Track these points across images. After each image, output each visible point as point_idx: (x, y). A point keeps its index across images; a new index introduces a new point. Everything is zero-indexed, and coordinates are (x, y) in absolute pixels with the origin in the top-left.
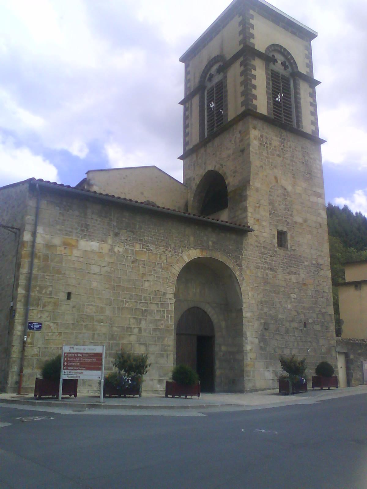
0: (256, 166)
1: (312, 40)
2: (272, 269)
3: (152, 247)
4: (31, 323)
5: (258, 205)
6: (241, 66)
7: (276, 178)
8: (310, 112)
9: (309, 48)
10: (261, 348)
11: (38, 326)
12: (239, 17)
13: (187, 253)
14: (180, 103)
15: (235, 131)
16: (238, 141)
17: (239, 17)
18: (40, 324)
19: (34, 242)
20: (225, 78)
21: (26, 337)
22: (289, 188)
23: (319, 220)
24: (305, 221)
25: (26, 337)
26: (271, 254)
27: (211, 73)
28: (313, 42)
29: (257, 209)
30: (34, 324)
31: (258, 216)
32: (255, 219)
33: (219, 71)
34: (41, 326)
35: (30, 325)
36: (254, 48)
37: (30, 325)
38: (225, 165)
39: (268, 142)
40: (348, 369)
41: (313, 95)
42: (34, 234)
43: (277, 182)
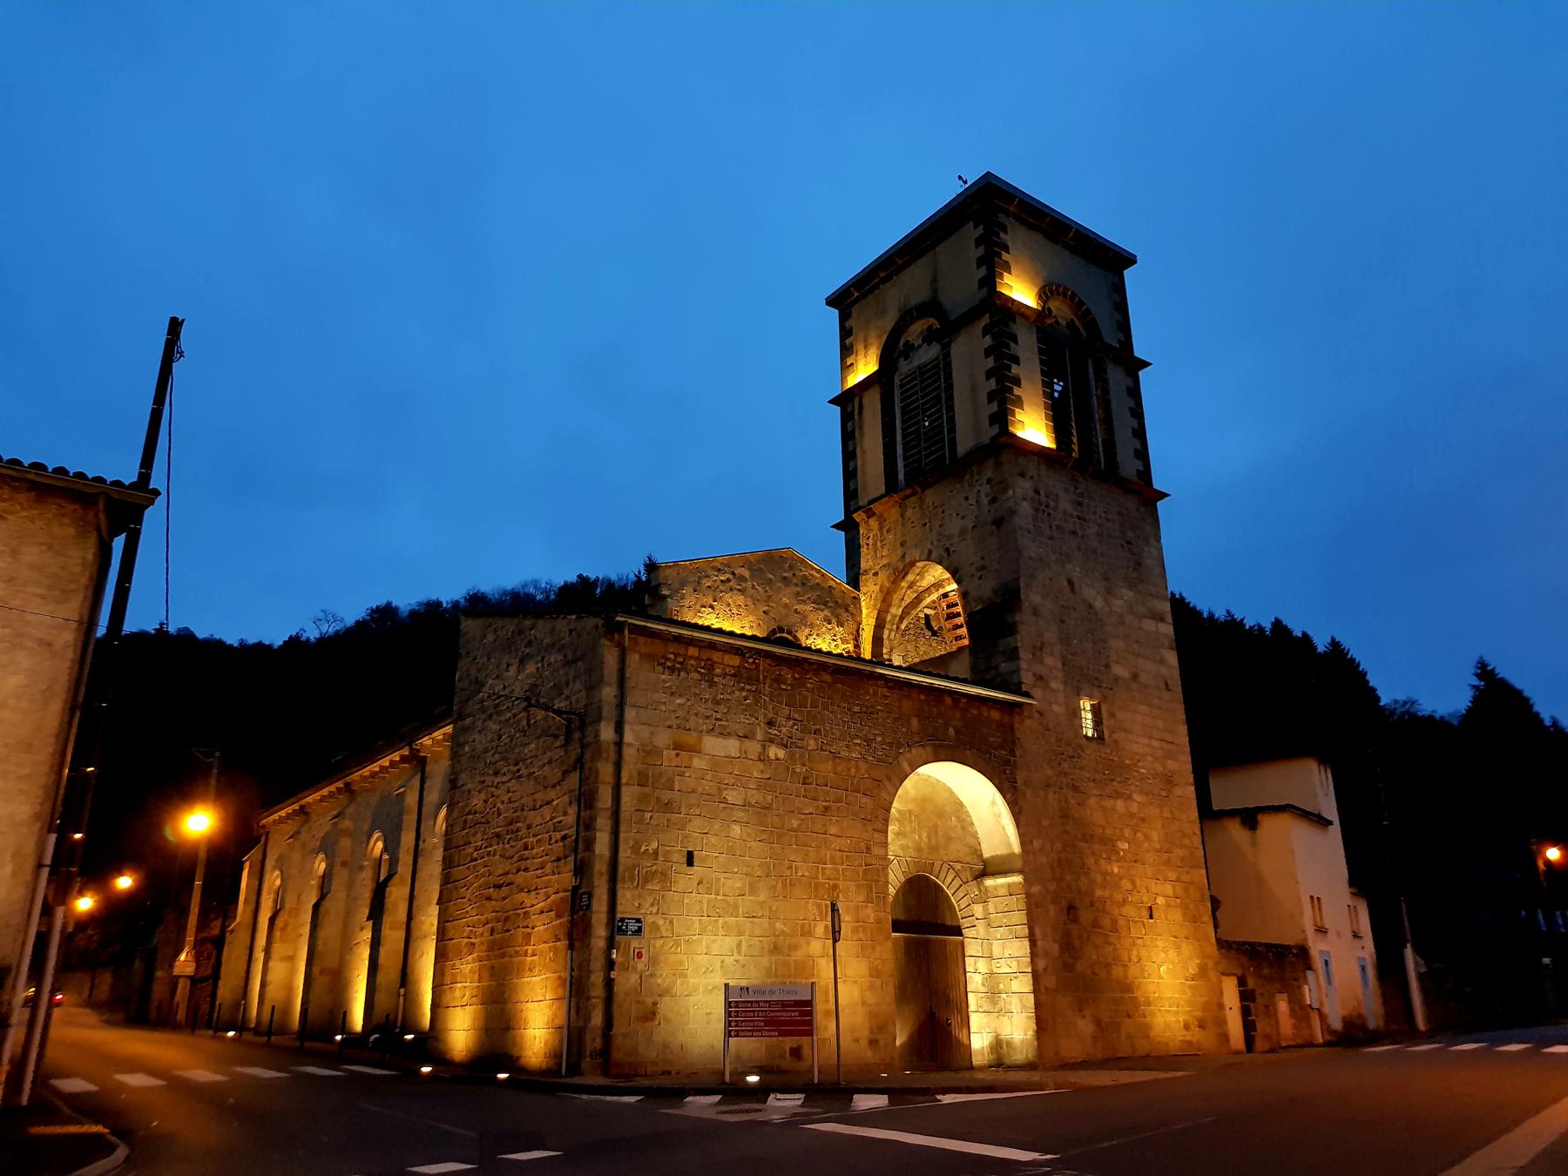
0: (1031, 558)
1: (1126, 268)
2: (1075, 789)
3: (839, 747)
4: (622, 920)
5: (1039, 644)
6: (985, 333)
7: (1070, 582)
8: (1131, 430)
9: (1119, 289)
10: (1065, 965)
11: (633, 926)
12: (975, 227)
13: (908, 755)
14: (833, 402)
15: (976, 478)
16: (985, 501)
17: (975, 227)
18: (638, 921)
19: (619, 744)
20: (947, 356)
21: (615, 951)
22: (1099, 603)
23: (1163, 671)
24: (1135, 677)
25: (615, 951)
26: (1071, 753)
27: (908, 341)
28: (1128, 274)
29: (1038, 653)
30: (627, 923)
31: (1040, 669)
32: (1034, 675)
33: (929, 337)
34: (641, 927)
35: (620, 924)
36: (1463, 715)
37: (620, 924)
38: (954, 551)
39: (1052, 504)
40: (1245, 1012)
41: (1135, 392)
42: (619, 728)
43: (1073, 591)
